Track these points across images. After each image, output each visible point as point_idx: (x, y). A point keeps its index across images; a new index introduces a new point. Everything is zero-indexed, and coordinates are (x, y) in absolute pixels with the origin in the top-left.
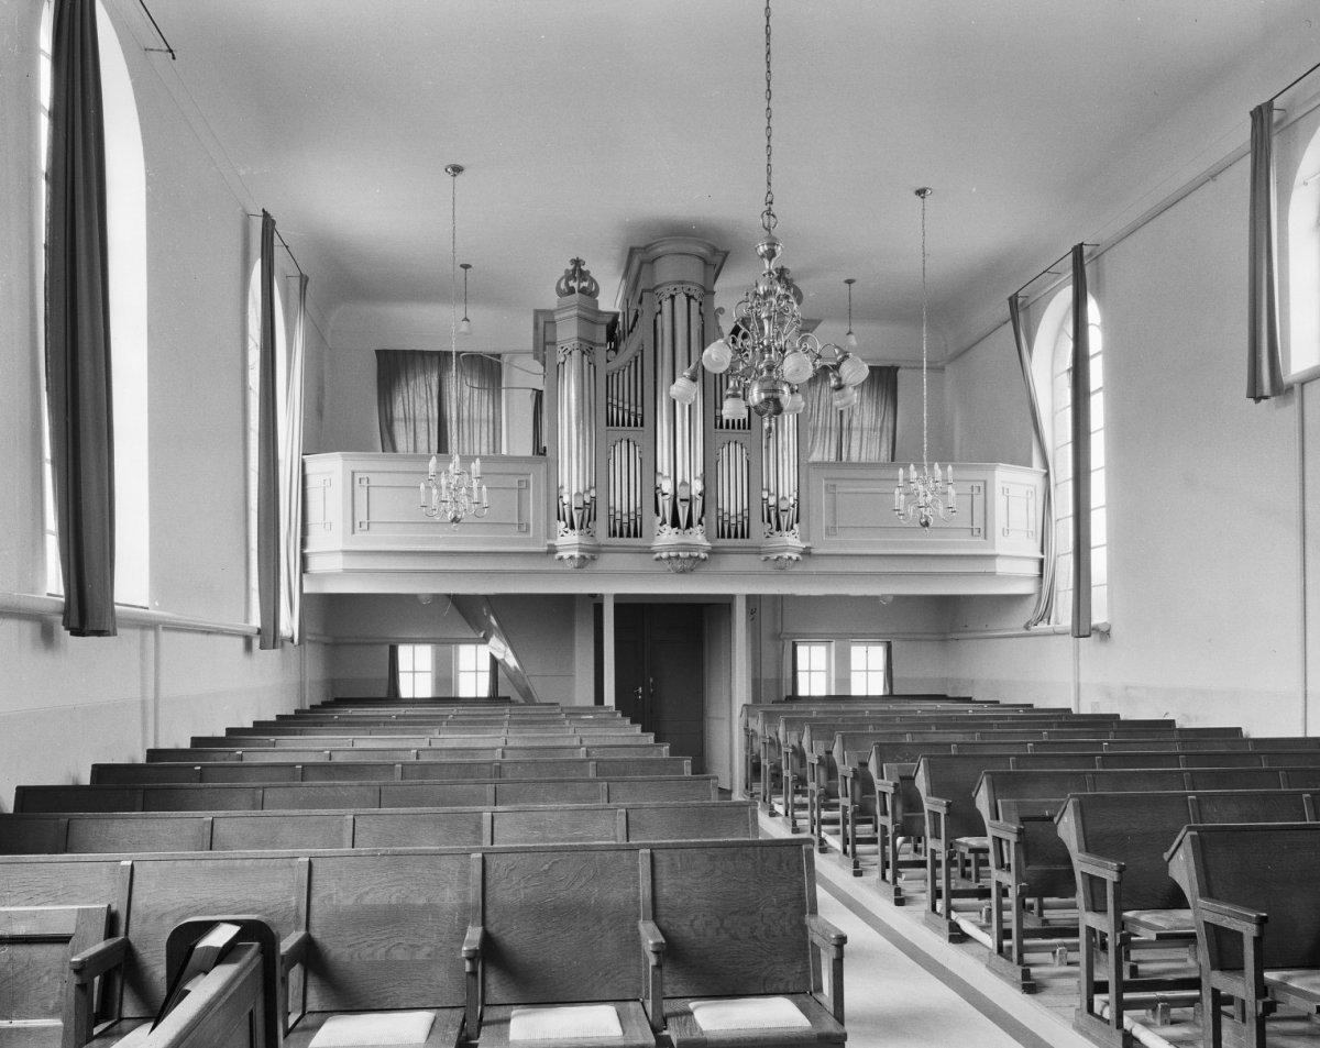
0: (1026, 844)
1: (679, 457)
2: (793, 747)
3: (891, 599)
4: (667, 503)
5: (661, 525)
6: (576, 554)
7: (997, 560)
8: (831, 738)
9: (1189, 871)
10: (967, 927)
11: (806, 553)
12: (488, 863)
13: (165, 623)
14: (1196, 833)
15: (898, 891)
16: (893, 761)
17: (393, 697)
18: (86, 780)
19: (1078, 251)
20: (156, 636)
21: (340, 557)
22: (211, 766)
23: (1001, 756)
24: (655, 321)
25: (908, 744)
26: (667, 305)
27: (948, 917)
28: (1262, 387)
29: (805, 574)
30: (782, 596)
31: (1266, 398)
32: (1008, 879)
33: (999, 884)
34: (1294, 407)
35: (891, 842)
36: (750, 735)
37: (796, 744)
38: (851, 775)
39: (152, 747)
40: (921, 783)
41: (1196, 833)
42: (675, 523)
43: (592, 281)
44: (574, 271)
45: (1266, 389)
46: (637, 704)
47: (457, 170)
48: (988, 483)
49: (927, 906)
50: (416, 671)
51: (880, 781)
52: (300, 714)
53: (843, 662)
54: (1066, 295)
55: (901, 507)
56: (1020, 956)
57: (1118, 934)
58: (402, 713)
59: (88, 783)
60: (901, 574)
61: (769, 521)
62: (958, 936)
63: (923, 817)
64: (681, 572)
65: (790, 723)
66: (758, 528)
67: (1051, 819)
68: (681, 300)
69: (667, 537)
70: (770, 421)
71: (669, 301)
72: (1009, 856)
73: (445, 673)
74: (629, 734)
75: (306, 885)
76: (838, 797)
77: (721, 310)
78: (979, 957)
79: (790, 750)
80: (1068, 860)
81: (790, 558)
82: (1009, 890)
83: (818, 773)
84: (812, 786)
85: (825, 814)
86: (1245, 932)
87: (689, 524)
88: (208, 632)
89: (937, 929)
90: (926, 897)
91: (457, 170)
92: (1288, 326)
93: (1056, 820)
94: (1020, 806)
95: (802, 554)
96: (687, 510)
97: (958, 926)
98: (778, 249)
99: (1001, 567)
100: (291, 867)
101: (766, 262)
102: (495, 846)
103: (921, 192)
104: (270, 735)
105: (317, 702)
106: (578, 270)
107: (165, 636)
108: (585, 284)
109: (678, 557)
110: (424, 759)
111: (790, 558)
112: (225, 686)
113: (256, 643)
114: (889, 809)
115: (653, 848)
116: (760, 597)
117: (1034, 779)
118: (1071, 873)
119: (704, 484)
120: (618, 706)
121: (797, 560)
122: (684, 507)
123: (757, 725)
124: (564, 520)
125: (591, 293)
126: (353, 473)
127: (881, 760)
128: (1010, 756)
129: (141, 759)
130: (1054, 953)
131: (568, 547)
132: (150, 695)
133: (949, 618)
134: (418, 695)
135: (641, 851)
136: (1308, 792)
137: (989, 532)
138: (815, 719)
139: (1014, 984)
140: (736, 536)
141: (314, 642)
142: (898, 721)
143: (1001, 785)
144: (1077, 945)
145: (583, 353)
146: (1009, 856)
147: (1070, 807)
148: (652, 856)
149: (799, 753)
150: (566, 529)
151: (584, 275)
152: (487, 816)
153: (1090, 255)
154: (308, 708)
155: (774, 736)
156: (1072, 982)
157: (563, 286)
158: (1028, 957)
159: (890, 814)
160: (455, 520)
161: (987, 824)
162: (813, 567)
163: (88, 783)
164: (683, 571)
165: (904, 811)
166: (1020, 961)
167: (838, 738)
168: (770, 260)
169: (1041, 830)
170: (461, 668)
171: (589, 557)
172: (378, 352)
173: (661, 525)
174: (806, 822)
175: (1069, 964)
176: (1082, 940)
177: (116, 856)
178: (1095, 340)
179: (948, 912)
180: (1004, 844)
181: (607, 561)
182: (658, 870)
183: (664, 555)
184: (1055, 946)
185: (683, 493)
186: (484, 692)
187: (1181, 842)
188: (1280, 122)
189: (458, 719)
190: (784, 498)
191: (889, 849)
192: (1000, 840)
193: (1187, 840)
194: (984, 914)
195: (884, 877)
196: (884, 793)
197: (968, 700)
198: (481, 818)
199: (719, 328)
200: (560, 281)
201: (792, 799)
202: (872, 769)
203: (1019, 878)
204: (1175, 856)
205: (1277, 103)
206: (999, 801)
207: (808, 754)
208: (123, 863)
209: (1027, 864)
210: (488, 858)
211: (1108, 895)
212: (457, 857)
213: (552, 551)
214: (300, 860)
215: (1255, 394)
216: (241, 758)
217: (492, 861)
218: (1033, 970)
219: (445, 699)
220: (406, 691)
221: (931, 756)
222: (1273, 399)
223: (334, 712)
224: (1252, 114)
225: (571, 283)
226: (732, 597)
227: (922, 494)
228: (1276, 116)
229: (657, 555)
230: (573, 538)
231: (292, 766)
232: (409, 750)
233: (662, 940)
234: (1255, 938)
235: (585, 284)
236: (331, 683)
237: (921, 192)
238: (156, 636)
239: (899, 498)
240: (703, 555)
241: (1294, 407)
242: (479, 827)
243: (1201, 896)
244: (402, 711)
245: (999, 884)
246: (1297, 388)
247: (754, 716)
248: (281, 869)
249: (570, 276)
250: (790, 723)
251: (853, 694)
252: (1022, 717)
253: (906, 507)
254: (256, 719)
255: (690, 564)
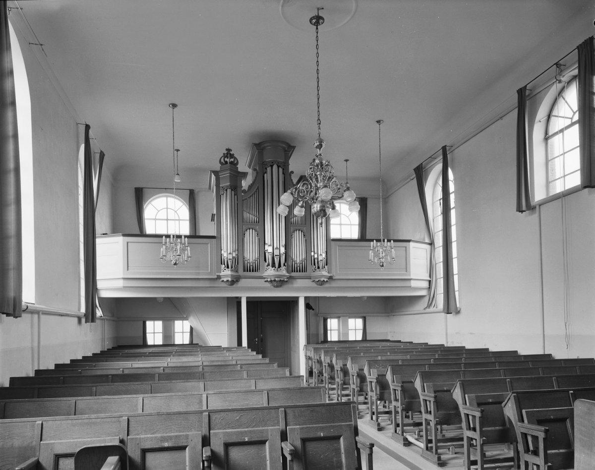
0: (438, 403)
1: (274, 238)
2: (328, 363)
3: (366, 298)
4: (270, 256)
5: (267, 266)
6: (230, 279)
7: (412, 281)
8: (346, 359)
9: (513, 410)
10: (411, 439)
11: (331, 278)
12: (211, 417)
13: (43, 311)
14: (515, 394)
15: (379, 425)
16: (374, 368)
17: (145, 345)
18: (7, 385)
19: (444, 149)
20: (39, 317)
21: (122, 281)
22: (67, 377)
23: (421, 365)
24: (264, 177)
25: (380, 360)
26: (269, 169)
27: (403, 435)
28: (522, 207)
29: (330, 287)
30: (319, 297)
31: (524, 211)
32: (431, 417)
33: (426, 420)
34: (537, 215)
35: (375, 403)
36: (308, 358)
37: (329, 362)
38: (356, 374)
39: (37, 369)
40: (389, 377)
41: (515, 394)
42: (273, 265)
43: (235, 158)
44: (227, 154)
45: (524, 208)
46: (257, 344)
47: (174, 106)
48: (407, 247)
49: (393, 431)
50: (154, 332)
51: (369, 377)
52: (102, 352)
53: (346, 325)
54: (439, 167)
55: (372, 259)
56: (436, 450)
57: (482, 439)
58: (151, 351)
59: (8, 386)
60: (386, 287)
61: (315, 265)
62: (407, 443)
63: (390, 392)
64: (277, 287)
65: (326, 353)
66: (310, 268)
67: (450, 391)
68: (275, 167)
69: (270, 272)
70: (322, 220)
71: (270, 168)
72: (430, 407)
73: (168, 333)
74: (254, 357)
75: (126, 428)
76: (350, 385)
77: (292, 172)
78: (417, 452)
79: (327, 365)
80: (456, 407)
81: (324, 281)
82: (431, 422)
83: (340, 374)
84: (337, 380)
85: (344, 392)
86: (539, 436)
87: (280, 266)
88: (62, 315)
89: (397, 441)
90: (392, 427)
91: (174, 106)
92: (533, 180)
93: (452, 391)
94: (434, 386)
95: (329, 279)
96: (278, 259)
97: (407, 439)
98: (324, 144)
99: (413, 284)
100: (119, 421)
101: (318, 150)
102: (270, 405)
103: (378, 122)
104: (93, 362)
105: (110, 347)
106: (229, 154)
107: (43, 317)
108: (232, 160)
109: (275, 280)
110: (167, 371)
111: (324, 281)
112: (76, 341)
113: (83, 320)
114: (374, 389)
115: (285, 407)
116: (309, 297)
117: (440, 374)
118: (459, 413)
119: (286, 249)
120: (249, 347)
121: (327, 281)
122: (277, 258)
123: (311, 354)
124: (224, 264)
125: (234, 164)
126: (128, 243)
127: (370, 368)
128: (425, 365)
129: (32, 374)
130: (449, 449)
131: (226, 276)
132: (36, 344)
133: (392, 306)
134: (156, 343)
135: (204, 414)
136: (509, 378)
137: (408, 269)
138: (337, 351)
139: (434, 463)
140: (300, 271)
141: (110, 320)
142: (372, 350)
143: (425, 377)
144: (463, 445)
145: (232, 190)
146: (430, 407)
147: (458, 385)
148: (285, 411)
149: (331, 366)
150: (226, 268)
151: (232, 156)
152: (204, 396)
153: (449, 150)
154: (106, 350)
155: (319, 359)
156: (462, 461)
157: (222, 160)
158: (439, 451)
159: (375, 392)
160: (175, 264)
161: (420, 394)
162: (334, 284)
163: (8, 386)
164: (277, 287)
165: (380, 390)
166: (436, 453)
167: (349, 359)
168: (320, 149)
169: (443, 396)
170: (176, 331)
171: (234, 281)
172: (136, 188)
173: (267, 266)
174: (336, 396)
175: (456, 453)
176: (465, 442)
177: (34, 419)
178: (452, 187)
179: (403, 432)
180: (428, 403)
181: (243, 283)
182: (288, 418)
183: (269, 280)
184: (449, 445)
185: (276, 252)
186: (187, 341)
187: (509, 398)
188: (529, 95)
189: (177, 354)
190: (321, 255)
191: (374, 407)
192: (426, 400)
193: (512, 398)
194: (416, 434)
195: (372, 419)
196: (371, 382)
197: (399, 341)
198: (202, 396)
199: (292, 180)
200: (221, 158)
201: (328, 386)
202: (366, 371)
203: (435, 417)
204: (507, 405)
205: (528, 87)
206: (425, 384)
207: (335, 366)
208: (37, 422)
209: (438, 411)
210: (210, 413)
211: (477, 422)
212: (196, 414)
213: (219, 277)
214: (123, 418)
215: (520, 210)
216: (81, 373)
217: (213, 417)
218: (442, 457)
219: (168, 344)
220: (150, 342)
221: (393, 365)
222: (527, 212)
223: (119, 351)
224: (518, 91)
225: (226, 159)
226: (298, 298)
227: (381, 253)
228: (527, 93)
229: (266, 280)
230: (228, 272)
231: (107, 376)
232: (160, 367)
233: (293, 448)
234: (544, 438)
235: (232, 160)
236: (116, 338)
237: (378, 122)
238: (39, 317)
239: (371, 253)
240: (286, 280)
241: (537, 215)
242: (201, 401)
243: (519, 422)
244: (151, 350)
245: (426, 420)
246: (537, 207)
247: (309, 350)
248: (115, 422)
249: (225, 156)
250: (326, 353)
251: (350, 339)
252: (424, 349)
253: (374, 259)
254: (92, 353)
255: (279, 283)
